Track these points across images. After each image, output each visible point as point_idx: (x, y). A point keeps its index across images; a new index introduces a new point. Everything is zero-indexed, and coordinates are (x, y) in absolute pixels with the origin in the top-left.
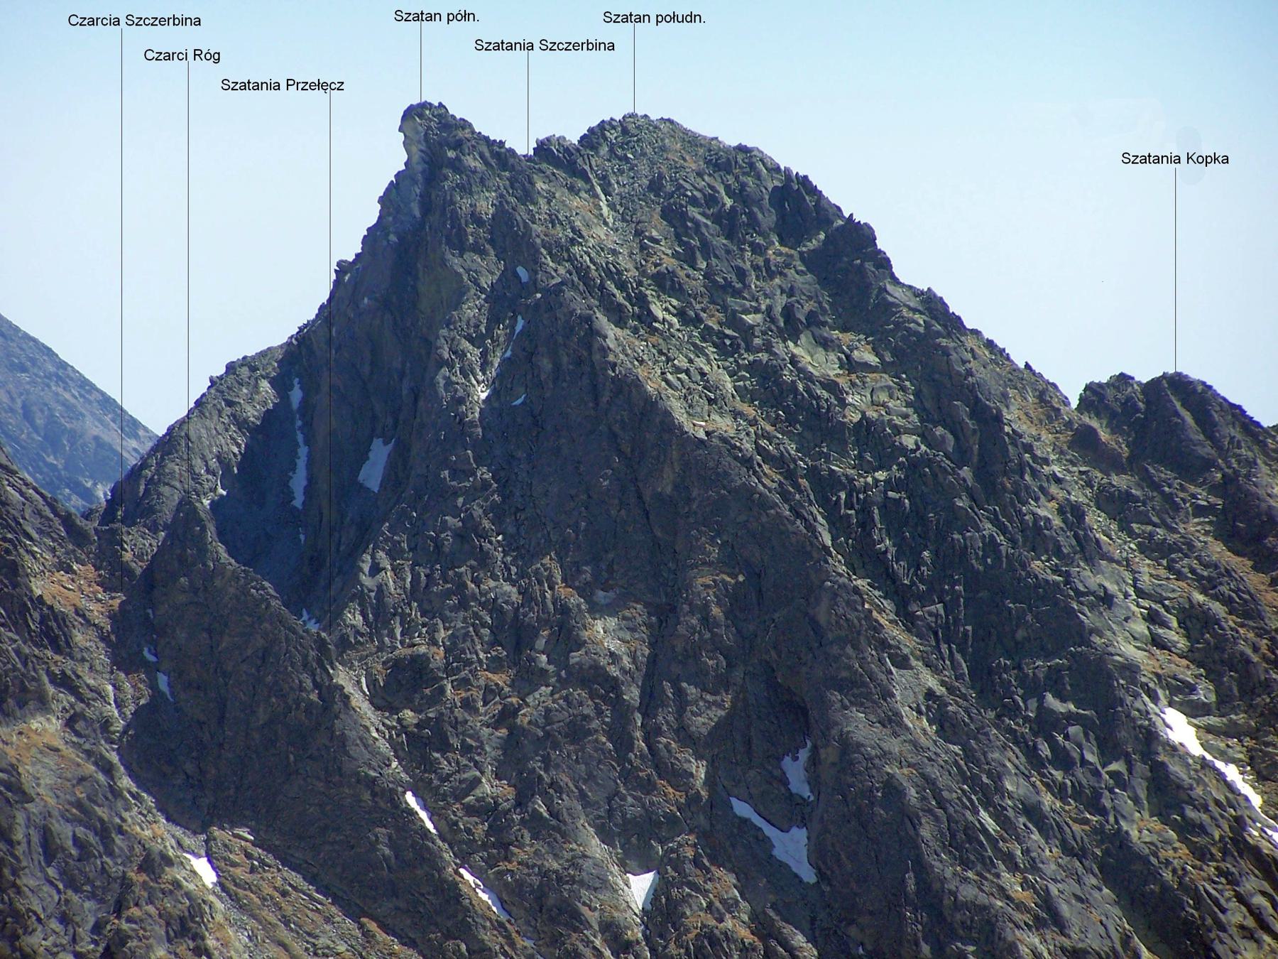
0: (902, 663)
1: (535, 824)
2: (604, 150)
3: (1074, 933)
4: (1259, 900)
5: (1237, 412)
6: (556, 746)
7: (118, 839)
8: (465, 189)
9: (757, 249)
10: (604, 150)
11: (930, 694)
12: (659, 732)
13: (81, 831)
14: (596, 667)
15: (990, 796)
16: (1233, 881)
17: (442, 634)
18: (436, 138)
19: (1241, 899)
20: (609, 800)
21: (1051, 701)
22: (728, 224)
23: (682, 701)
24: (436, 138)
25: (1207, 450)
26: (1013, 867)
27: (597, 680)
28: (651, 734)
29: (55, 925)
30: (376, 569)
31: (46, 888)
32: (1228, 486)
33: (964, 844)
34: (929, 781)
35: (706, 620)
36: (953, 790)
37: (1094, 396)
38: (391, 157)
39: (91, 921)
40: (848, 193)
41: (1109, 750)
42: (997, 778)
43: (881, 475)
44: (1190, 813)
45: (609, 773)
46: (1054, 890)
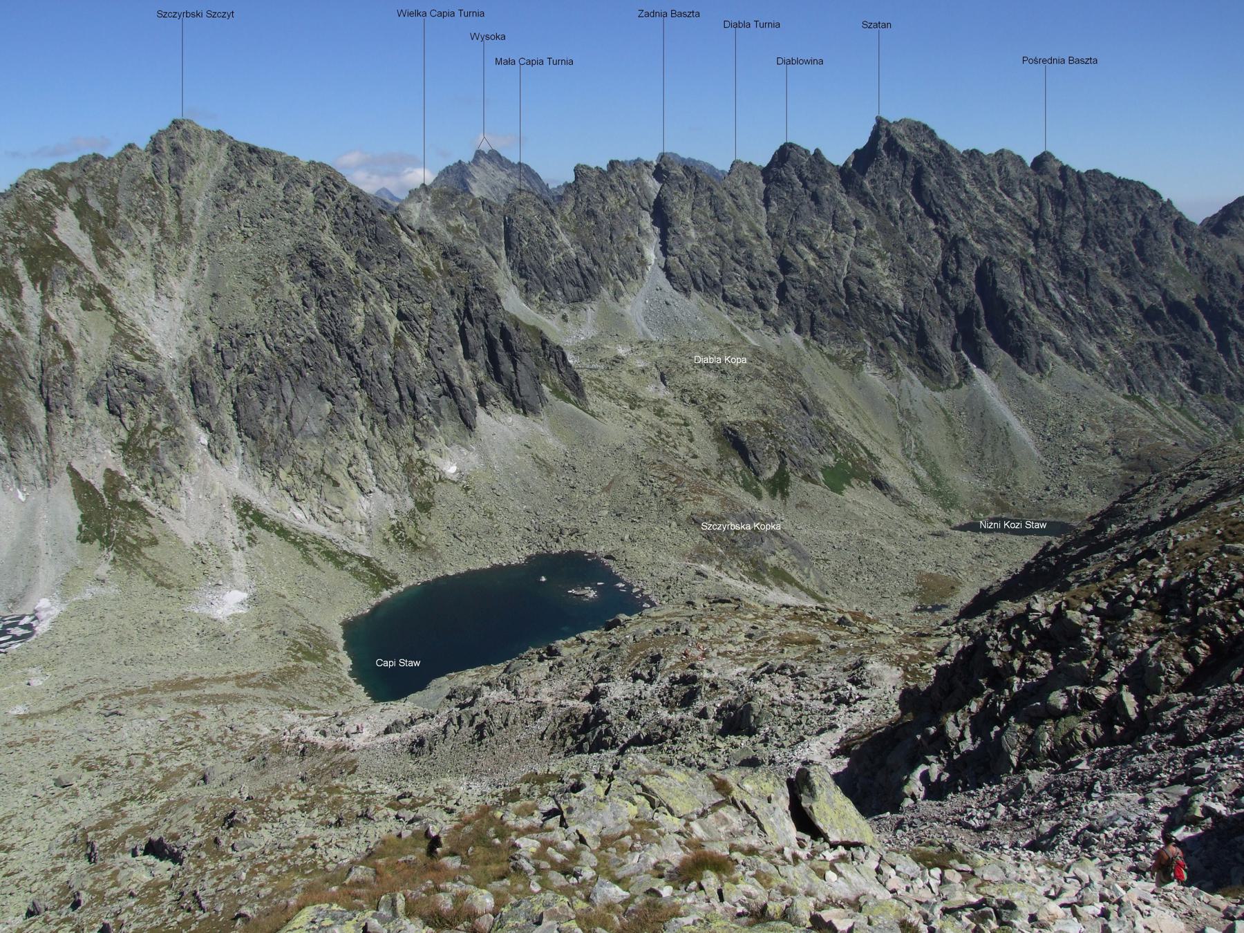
18: (879, 121)
24: (879, 121)
27: (896, 181)
33: (938, 196)
38: (875, 122)
40: (931, 126)
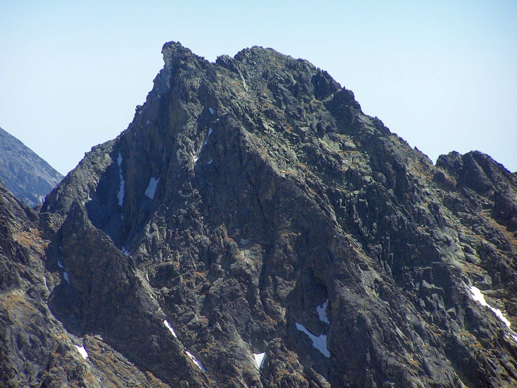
0: (365, 268)
1: (217, 333)
2: (244, 61)
3: (435, 377)
4: (509, 364)
5: (500, 167)
6: (225, 302)
7: (48, 340)
8: (188, 77)
9: (306, 101)
10: (244, 61)
11: (376, 281)
12: (266, 296)
13: (33, 336)
14: (241, 270)
15: (400, 322)
16: (499, 357)
17: (179, 257)
18: (176, 56)
19: (502, 364)
20: (247, 324)
21: (425, 284)
22: (295, 91)
23: (276, 284)
24: (176, 56)
25: (488, 182)
26: (410, 351)
27: (241, 275)
28: (263, 297)
29: (22, 374)
30: (152, 230)
31: (19, 359)
32: (497, 197)
33: (390, 341)
34: (376, 316)
35: (286, 251)
36: (386, 320)
37: (443, 160)
38: (158, 64)
39: (37, 373)
40: (343, 78)
41: (449, 303)
42: (403, 315)
43: (356, 192)
44: (482, 329)
45: (246, 313)
46: (426, 360)
